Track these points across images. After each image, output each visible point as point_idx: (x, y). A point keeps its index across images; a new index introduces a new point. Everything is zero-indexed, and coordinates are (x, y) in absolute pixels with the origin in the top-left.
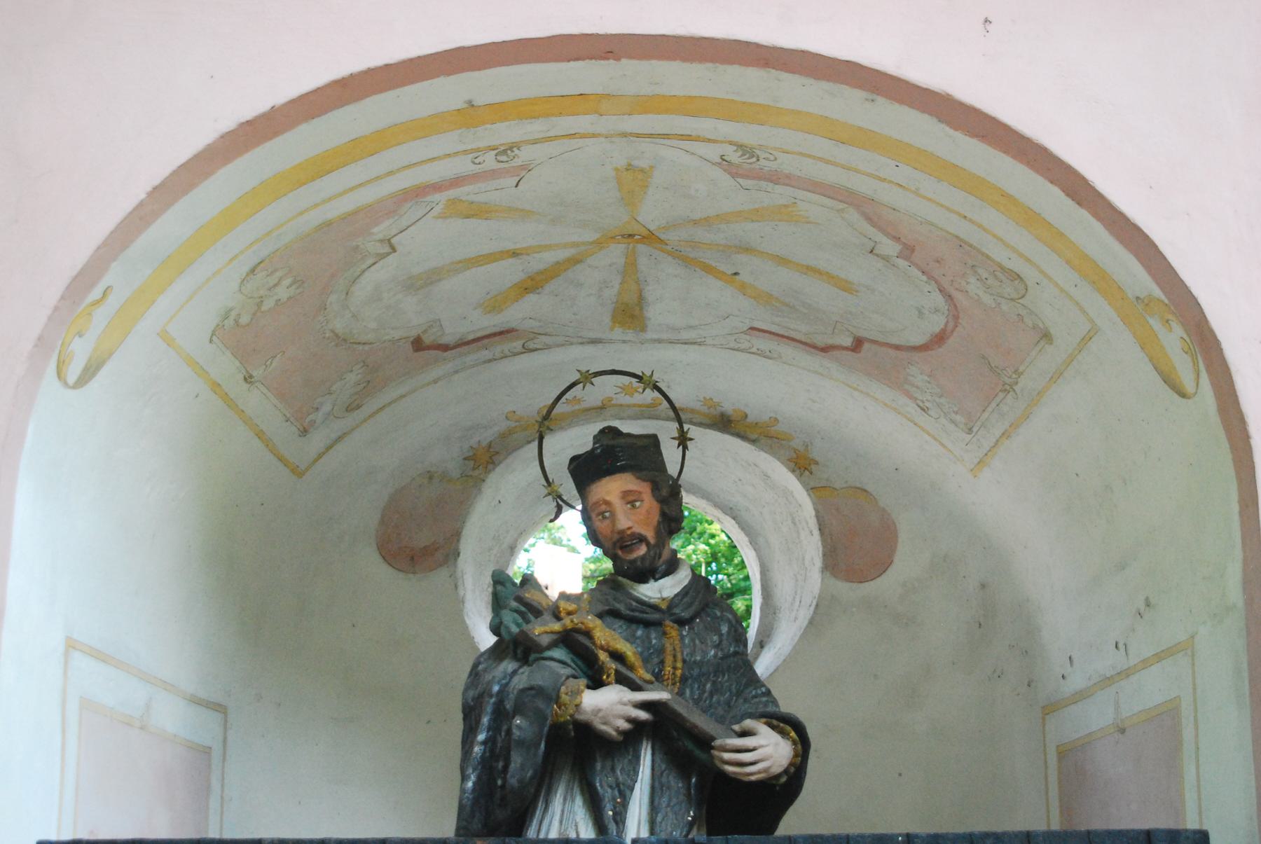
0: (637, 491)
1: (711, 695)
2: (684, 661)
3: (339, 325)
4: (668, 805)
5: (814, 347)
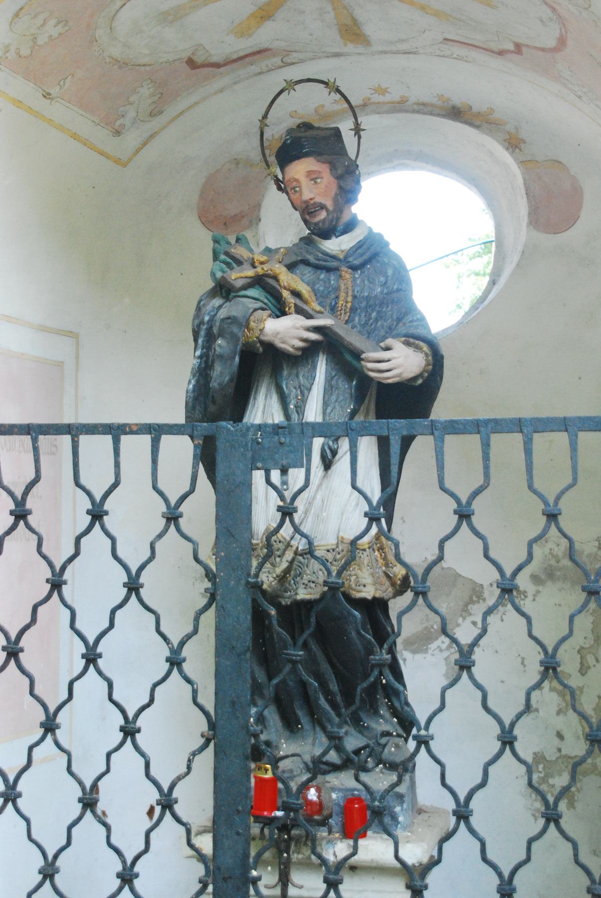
0: (317, 171)
1: (376, 320)
2: (354, 297)
3: (116, 51)
4: (336, 401)
5: (493, 52)
